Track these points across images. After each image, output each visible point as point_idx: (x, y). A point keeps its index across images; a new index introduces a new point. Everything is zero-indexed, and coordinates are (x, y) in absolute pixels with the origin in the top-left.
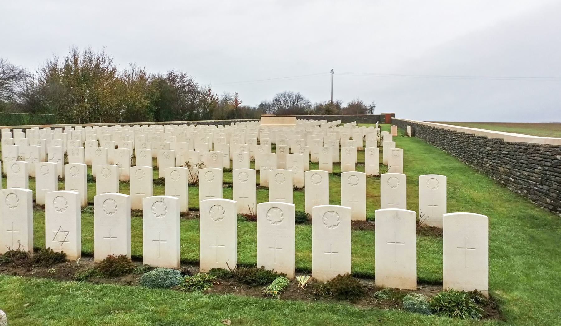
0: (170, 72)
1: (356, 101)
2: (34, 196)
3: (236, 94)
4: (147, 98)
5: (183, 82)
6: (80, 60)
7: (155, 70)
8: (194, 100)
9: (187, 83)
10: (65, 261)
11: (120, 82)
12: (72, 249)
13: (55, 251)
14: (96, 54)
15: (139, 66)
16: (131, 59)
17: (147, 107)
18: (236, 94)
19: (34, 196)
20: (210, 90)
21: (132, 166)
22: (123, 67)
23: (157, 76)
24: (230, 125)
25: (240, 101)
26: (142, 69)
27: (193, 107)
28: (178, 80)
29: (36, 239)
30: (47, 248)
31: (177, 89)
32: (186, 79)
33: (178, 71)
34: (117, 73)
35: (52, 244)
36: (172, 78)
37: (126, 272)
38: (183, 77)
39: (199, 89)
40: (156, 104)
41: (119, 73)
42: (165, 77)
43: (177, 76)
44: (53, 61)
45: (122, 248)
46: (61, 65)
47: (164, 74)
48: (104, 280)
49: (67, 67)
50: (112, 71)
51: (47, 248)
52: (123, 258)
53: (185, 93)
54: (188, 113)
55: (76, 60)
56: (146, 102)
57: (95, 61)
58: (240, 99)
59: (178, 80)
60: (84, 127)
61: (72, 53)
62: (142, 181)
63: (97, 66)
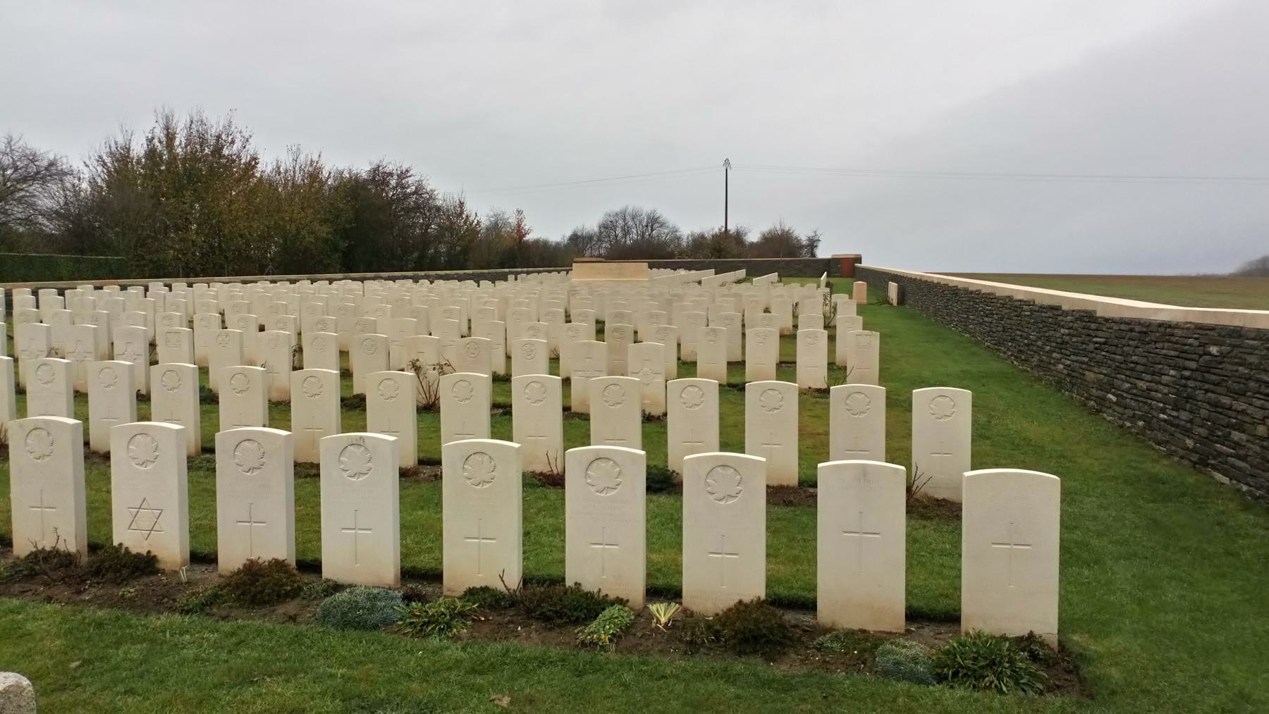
0: (374, 166)
3: (520, 212)
4: (326, 221)
5: (403, 187)
7: (345, 159)
8: (428, 226)
11: (267, 185)
12: (168, 542)
13: (134, 551)
14: (215, 125)
15: (309, 153)
16: (292, 135)
17: (326, 241)
18: (520, 212)
20: (461, 204)
22: (272, 153)
26: (315, 158)
28: (393, 182)
32: (410, 180)
33: (392, 163)
34: (260, 167)
36: (379, 178)
38: (403, 175)
39: (439, 203)
40: (346, 234)
41: (265, 166)
43: (391, 174)
44: (121, 141)
45: (276, 545)
46: (138, 149)
47: (362, 168)
49: (151, 153)
51: (116, 544)
52: (278, 565)
53: (408, 211)
54: (415, 255)
55: (170, 137)
56: (324, 231)
57: (213, 142)
58: (527, 225)
59: (393, 182)
60: (124, 288)
61: (162, 123)
63: (218, 150)
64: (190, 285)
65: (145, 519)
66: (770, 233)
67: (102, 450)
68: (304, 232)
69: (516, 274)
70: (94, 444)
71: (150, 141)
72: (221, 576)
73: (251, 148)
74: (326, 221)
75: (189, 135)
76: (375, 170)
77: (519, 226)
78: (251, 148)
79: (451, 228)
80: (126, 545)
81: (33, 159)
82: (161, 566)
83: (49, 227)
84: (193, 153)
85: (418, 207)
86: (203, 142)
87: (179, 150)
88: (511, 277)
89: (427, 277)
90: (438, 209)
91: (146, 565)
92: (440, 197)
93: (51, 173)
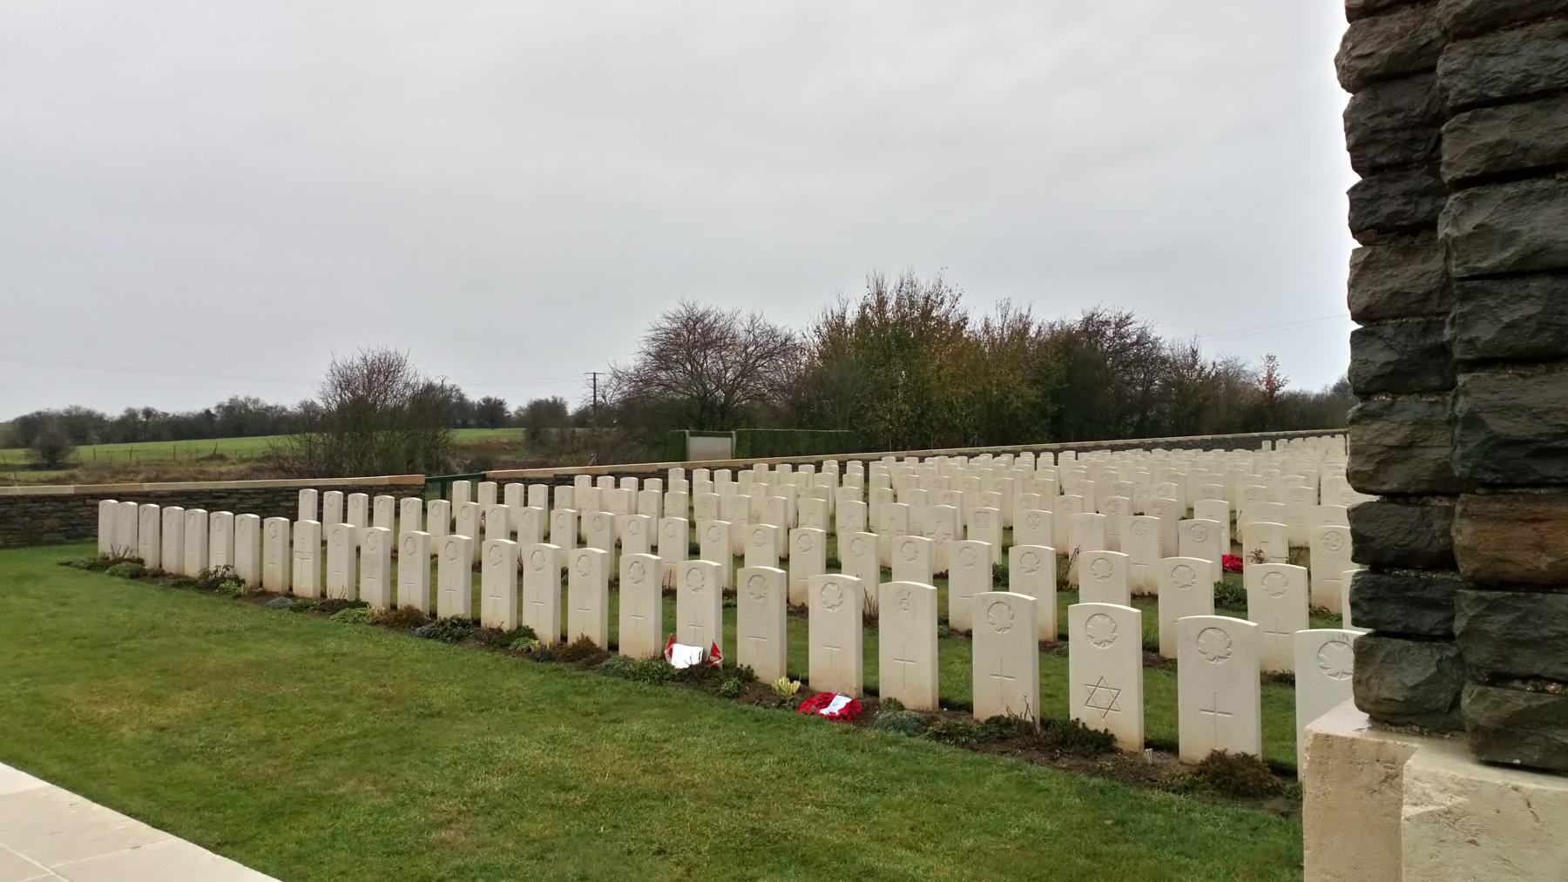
0: (1088, 314)
1: (683, 310)
2: (943, 601)
3: (1271, 358)
4: (1035, 382)
5: (1122, 337)
6: (891, 304)
7: (1055, 310)
8: (1151, 382)
9: (1135, 337)
10: (1114, 751)
11: (973, 346)
12: (1128, 726)
13: (1091, 727)
14: (925, 285)
15: (1019, 307)
16: (1004, 292)
17: (1034, 405)
18: (1271, 358)
19: (943, 601)
20: (1194, 353)
21: (1165, 555)
22: (980, 310)
23: (996, 323)
24: (1260, 447)
25: (1281, 378)
26: (1025, 313)
27: (1147, 401)
28: (1110, 333)
29: (866, 674)
30: (1072, 718)
31: (1106, 354)
32: (1131, 328)
33: (1109, 310)
34: (969, 327)
35: (1084, 710)
36: (1092, 328)
37: (1268, 791)
38: (1122, 323)
39: (1164, 353)
40: (1055, 396)
41: (974, 325)
42: (1077, 327)
43: (1107, 323)
44: (837, 311)
45: (1243, 737)
46: (851, 318)
47: (1073, 318)
48: (1224, 801)
49: (863, 320)
50: (958, 324)
51: (1072, 718)
52: (1246, 759)
53: (1127, 365)
54: (1136, 418)
55: (882, 302)
56: (1032, 394)
57: (921, 302)
58: (1280, 374)
59: (1110, 333)
60: (922, 460)
61: (873, 290)
62: (808, 557)
63: (926, 314)
64: (922, 460)
65: (1103, 697)
66: (69, 412)
67: (963, 627)
68: (1011, 397)
69: (1274, 440)
70: (954, 620)
71: (863, 308)
72: (1182, 763)
73: (961, 308)
74: (1035, 382)
75: (900, 298)
76: (1088, 321)
77: (1270, 376)
78: (961, 308)
79: (1180, 384)
80: (1083, 719)
81: (772, 334)
82: (1119, 745)
83: (777, 401)
84: (904, 316)
85: (1139, 361)
86: (912, 305)
87: (890, 315)
88: (1266, 444)
89: (1284, 437)
90: (1164, 360)
91: (1104, 742)
92: (1166, 345)
93: (786, 348)
